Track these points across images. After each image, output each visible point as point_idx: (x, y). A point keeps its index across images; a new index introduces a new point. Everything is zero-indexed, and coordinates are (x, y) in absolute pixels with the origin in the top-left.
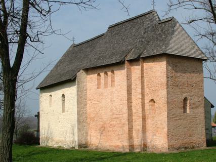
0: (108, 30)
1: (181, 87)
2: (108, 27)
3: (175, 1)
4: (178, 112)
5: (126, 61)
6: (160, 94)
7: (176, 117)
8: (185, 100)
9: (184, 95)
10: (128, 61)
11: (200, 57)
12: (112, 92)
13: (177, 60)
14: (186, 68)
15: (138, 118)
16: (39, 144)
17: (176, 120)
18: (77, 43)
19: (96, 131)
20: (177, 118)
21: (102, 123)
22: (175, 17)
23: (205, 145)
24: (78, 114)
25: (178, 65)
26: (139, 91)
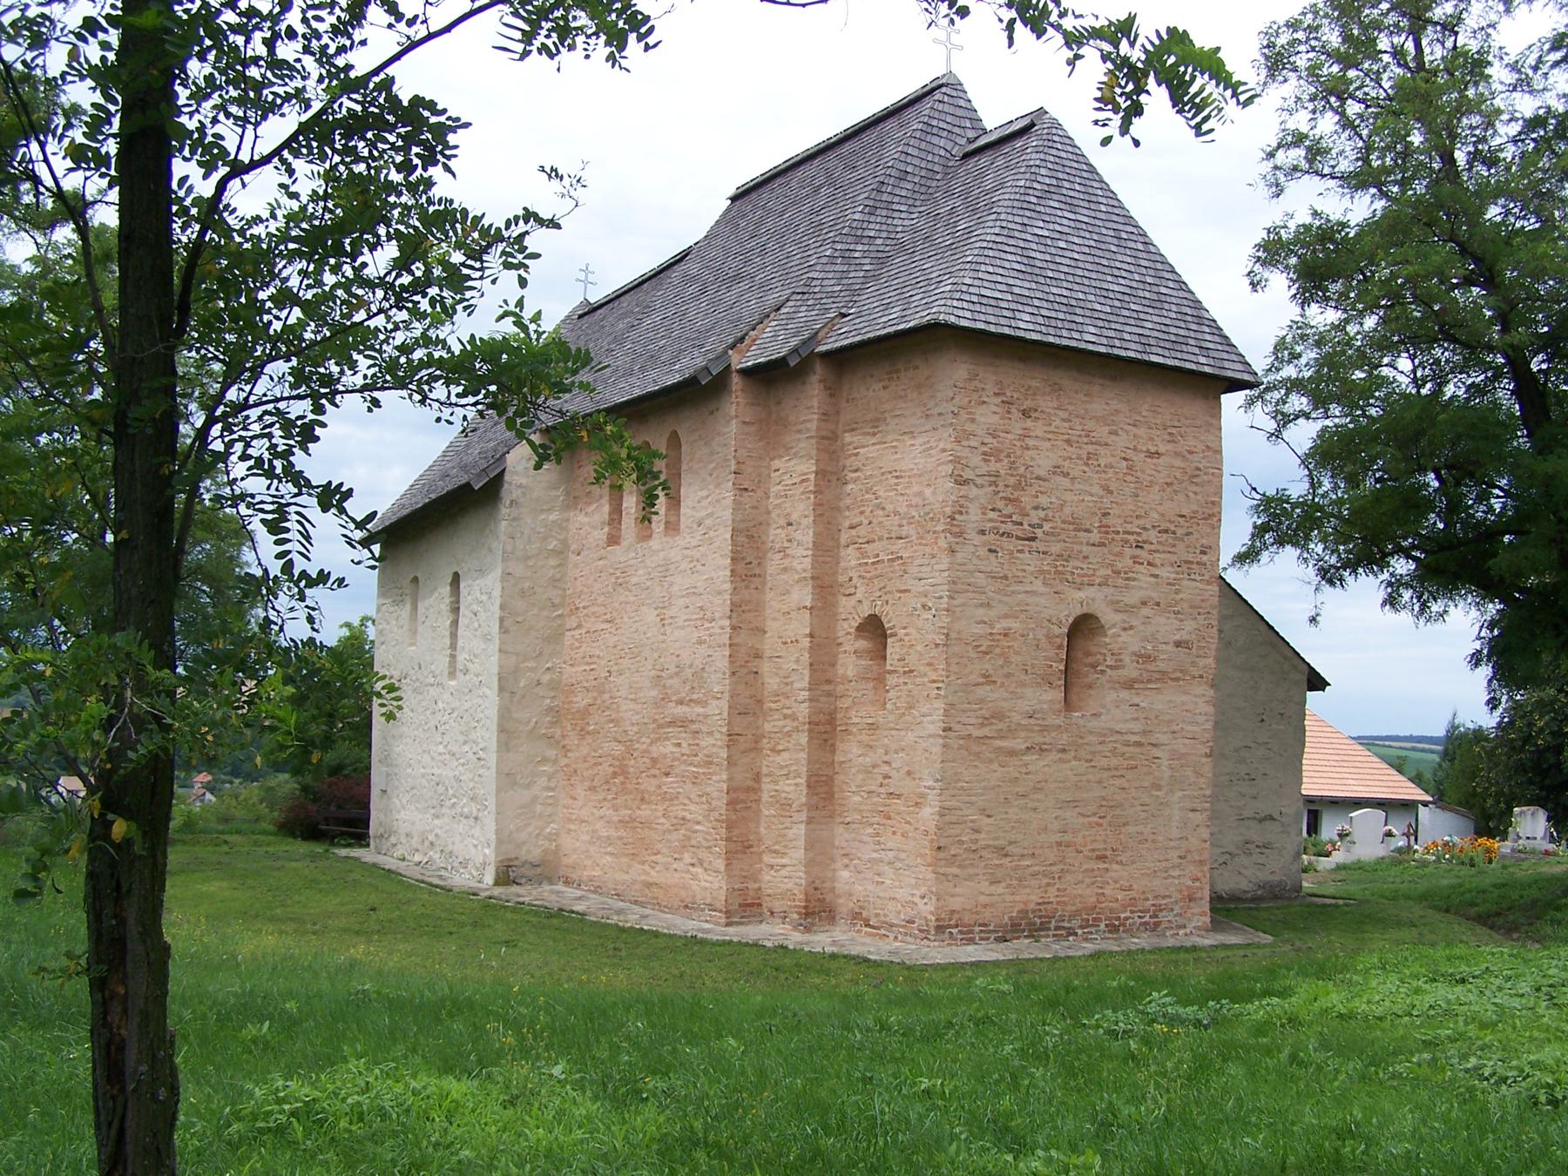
0: (726, 220)
1: (1056, 548)
2: (732, 191)
3: (1566, 514)
4: (1023, 705)
5: (736, 380)
6: (919, 587)
7: (1010, 732)
8: (1083, 627)
9: (1077, 601)
10: (745, 372)
11: (1204, 365)
12: (666, 569)
13: (1032, 380)
14: (1102, 432)
15: (789, 725)
16: (1311, 689)
17: (1012, 753)
18: (595, 297)
19: (592, 789)
20: (1019, 744)
21: (618, 749)
22: (1053, 112)
23: (1200, 915)
24: (501, 689)
25: (1047, 403)
26: (802, 559)
